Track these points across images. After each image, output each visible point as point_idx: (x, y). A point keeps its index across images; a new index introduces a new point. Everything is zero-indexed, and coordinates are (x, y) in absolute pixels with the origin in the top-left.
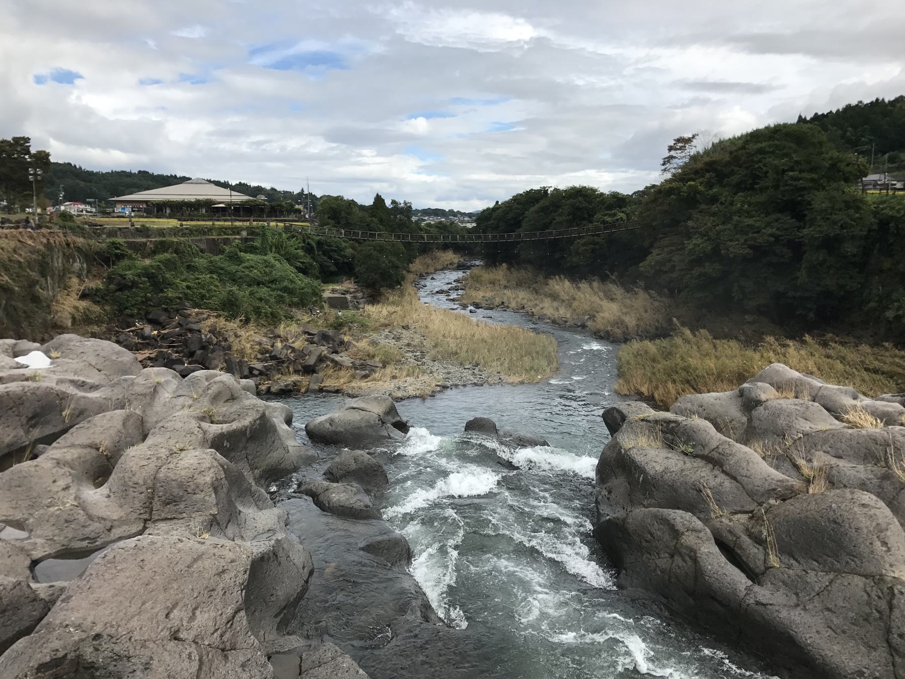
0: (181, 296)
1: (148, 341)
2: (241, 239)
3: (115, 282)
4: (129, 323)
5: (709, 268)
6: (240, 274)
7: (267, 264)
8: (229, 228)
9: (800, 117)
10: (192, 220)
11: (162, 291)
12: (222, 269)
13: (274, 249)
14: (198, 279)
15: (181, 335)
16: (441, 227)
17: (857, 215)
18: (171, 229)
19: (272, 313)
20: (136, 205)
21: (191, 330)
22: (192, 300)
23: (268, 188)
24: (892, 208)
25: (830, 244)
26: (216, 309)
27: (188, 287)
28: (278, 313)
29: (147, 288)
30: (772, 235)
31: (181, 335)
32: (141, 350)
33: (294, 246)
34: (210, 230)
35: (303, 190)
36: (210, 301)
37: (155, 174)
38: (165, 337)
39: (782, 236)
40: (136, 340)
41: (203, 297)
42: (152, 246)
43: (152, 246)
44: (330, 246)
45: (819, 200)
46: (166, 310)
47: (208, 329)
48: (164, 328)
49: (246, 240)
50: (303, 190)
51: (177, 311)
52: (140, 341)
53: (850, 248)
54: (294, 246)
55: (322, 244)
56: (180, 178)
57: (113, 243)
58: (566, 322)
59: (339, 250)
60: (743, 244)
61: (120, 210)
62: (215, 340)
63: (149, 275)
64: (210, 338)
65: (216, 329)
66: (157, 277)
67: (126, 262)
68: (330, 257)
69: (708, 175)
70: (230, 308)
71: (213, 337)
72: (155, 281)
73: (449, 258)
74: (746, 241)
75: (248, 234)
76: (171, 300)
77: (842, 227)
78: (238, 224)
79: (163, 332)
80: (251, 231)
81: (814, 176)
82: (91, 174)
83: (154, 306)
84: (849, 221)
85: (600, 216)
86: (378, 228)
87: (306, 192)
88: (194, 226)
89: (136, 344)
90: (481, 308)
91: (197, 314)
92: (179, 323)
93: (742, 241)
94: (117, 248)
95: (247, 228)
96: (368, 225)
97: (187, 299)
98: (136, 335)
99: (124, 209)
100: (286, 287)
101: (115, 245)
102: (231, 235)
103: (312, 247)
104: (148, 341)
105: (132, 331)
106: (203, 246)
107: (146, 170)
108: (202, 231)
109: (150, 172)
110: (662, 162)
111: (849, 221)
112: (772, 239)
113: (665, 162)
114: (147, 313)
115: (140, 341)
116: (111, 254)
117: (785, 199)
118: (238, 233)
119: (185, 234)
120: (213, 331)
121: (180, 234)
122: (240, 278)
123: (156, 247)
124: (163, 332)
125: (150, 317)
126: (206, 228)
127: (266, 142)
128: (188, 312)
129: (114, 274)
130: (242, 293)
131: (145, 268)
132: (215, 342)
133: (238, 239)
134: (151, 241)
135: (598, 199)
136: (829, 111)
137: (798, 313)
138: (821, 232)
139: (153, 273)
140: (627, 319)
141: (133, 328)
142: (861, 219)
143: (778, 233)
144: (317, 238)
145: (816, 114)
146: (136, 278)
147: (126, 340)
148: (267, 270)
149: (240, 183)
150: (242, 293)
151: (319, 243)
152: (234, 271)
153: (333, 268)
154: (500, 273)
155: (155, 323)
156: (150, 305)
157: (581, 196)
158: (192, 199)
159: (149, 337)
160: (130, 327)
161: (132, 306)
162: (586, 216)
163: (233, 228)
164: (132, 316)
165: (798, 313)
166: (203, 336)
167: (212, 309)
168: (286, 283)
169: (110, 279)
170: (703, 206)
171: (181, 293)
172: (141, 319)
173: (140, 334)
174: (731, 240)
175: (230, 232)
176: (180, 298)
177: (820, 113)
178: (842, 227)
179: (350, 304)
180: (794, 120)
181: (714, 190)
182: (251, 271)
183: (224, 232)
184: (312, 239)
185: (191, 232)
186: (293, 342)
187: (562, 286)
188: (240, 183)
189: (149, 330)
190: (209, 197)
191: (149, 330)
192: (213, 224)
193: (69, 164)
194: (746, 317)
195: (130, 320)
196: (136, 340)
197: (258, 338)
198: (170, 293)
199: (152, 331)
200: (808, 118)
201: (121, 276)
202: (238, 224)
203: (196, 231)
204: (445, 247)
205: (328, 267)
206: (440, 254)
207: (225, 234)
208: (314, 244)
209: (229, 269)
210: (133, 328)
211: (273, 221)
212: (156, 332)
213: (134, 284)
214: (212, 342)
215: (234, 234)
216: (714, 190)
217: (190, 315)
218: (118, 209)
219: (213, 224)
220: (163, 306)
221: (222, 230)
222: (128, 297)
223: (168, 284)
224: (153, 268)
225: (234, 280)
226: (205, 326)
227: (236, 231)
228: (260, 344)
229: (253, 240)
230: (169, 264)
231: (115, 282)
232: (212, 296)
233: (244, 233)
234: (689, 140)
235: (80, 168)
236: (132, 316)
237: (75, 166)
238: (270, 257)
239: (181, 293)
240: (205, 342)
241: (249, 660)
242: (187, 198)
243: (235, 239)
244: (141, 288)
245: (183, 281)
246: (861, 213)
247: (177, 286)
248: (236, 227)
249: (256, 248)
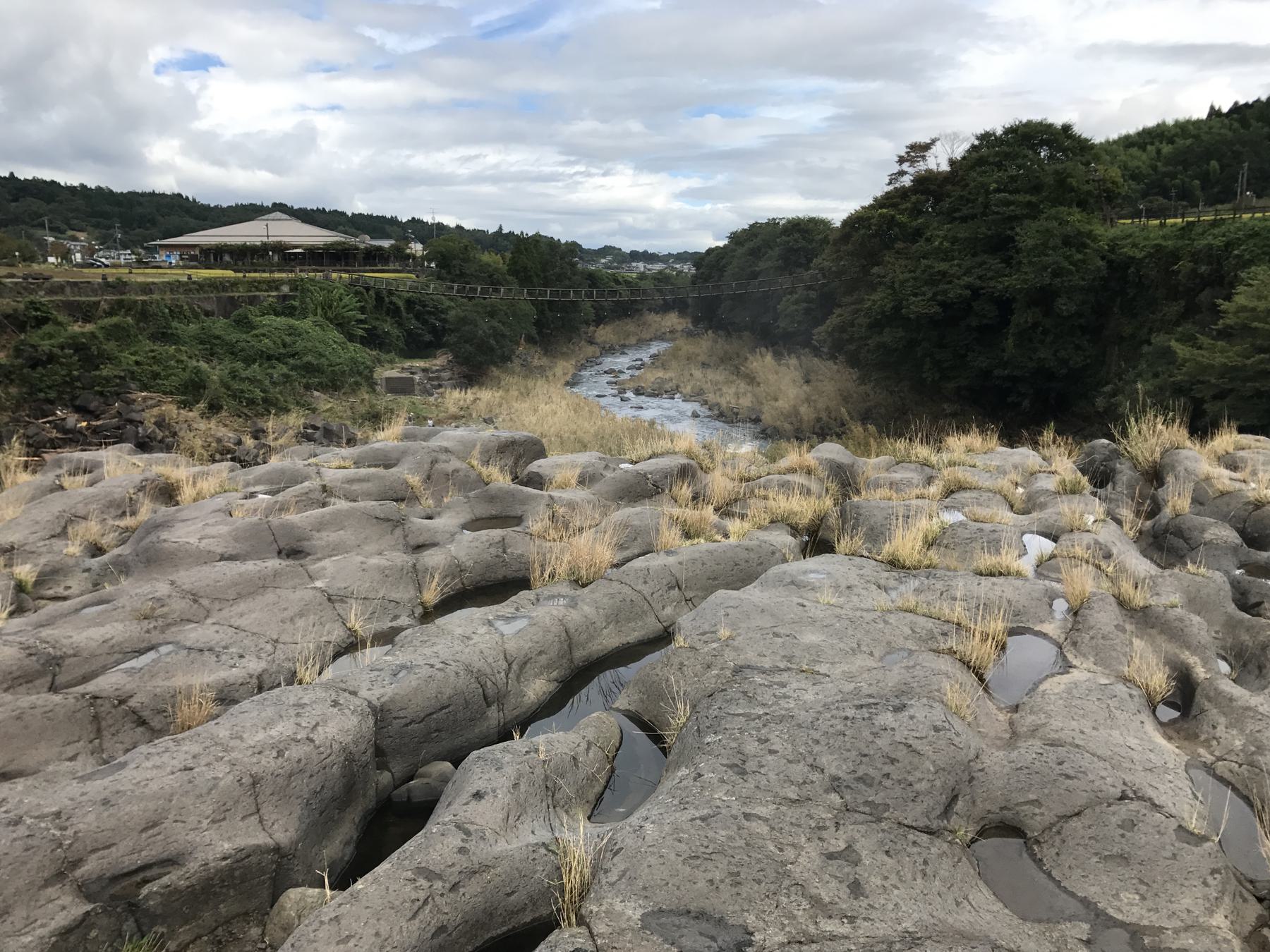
0: (122, 374)
1: (71, 436)
2: (278, 297)
3: (25, 354)
4: (43, 410)
5: (887, 337)
6: (244, 344)
7: (292, 331)
8: (264, 282)
9: (1212, 108)
10: (255, 271)
11: (97, 368)
12: (218, 337)
13: (319, 311)
14: (153, 351)
15: (119, 428)
16: (661, 278)
17: (1080, 256)
18: (168, 283)
19: (265, 400)
20: (185, 251)
21: (131, 421)
22: (140, 380)
23: (453, 225)
24: (1134, 245)
25: (1043, 298)
26: (172, 393)
27: (137, 363)
28: (277, 399)
29: (73, 364)
30: (968, 287)
31: (119, 428)
32: (60, 447)
33: (350, 306)
34: (234, 284)
35: (501, 228)
36: (165, 382)
37: (225, 205)
38: (98, 430)
39: (983, 288)
40: (54, 434)
41: (156, 376)
42: (106, 307)
43: (106, 307)
44: (424, 306)
45: (1027, 235)
46: (101, 394)
47: (153, 420)
48: (97, 418)
49: (285, 297)
50: (501, 228)
51: (118, 394)
52: (59, 435)
53: (1065, 306)
54: (350, 306)
55: (414, 303)
56: (330, 212)
57: (32, 303)
58: (737, 414)
59: (438, 311)
60: (929, 300)
61: (164, 258)
62: (160, 435)
63: (79, 347)
64: (153, 431)
65: (164, 420)
66: (90, 349)
67: (47, 328)
68: (425, 322)
69: (914, 198)
70: (192, 391)
71: (157, 431)
72: (84, 351)
73: (669, 324)
74: (935, 294)
75: (291, 290)
76: (107, 379)
77: (1055, 274)
78: (277, 275)
79: (94, 423)
80: (294, 284)
81: (1034, 199)
82: (207, 208)
83: (83, 388)
84: (1066, 264)
85: (820, 261)
86: (506, 280)
87: (505, 231)
88: (206, 279)
89: (51, 440)
90: (643, 394)
91: (145, 399)
92: (118, 412)
93: (930, 295)
94: (37, 309)
95: (290, 282)
96: (490, 276)
97: (133, 379)
98: (54, 428)
99: (169, 256)
100: (309, 363)
101: (33, 305)
102: (267, 291)
103: (398, 308)
104: (71, 436)
105: (49, 422)
106: (209, 307)
107: (283, 202)
108: (214, 285)
109: (289, 205)
110: (887, 181)
111: (1066, 264)
112: (968, 292)
113: (891, 180)
114: (74, 398)
115: (59, 435)
116: (29, 318)
117: (990, 233)
118: (277, 289)
119: (190, 290)
120: (160, 423)
121: (181, 290)
122: (242, 350)
123: (112, 308)
124: (94, 423)
125: (78, 403)
126: (228, 281)
127: (477, 157)
128: (133, 396)
129: (23, 345)
130: (215, 372)
131: (74, 337)
132: (159, 438)
133: (273, 296)
134: (106, 300)
135: (820, 237)
136: (1255, 99)
137: (1009, 400)
138: (1025, 281)
139: (83, 343)
140: (803, 409)
141: (50, 418)
142: (1084, 261)
143: (978, 282)
144: (406, 295)
145: (1236, 103)
146: (55, 350)
147: (37, 434)
148: (288, 339)
149: (413, 218)
150: (215, 372)
151: (409, 303)
152: (234, 340)
153: (428, 337)
154: (705, 344)
155: (83, 411)
156: (78, 387)
157: (799, 231)
158: (257, 241)
159: (73, 431)
160: (47, 416)
161: (50, 388)
162: (803, 261)
163: (269, 282)
164: (51, 402)
165: (1009, 400)
166: (140, 430)
167: (165, 393)
168: (309, 358)
169: (18, 352)
170: (899, 245)
171: (124, 370)
172: (65, 406)
173: (59, 426)
174: (916, 295)
175: (265, 287)
176: (121, 378)
177: (1242, 102)
178: (1055, 274)
179: (417, 388)
180: (1203, 114)
181: (919, 221)
182: (260, 341)
183: (256, 287)
184: (399, 297)
185: (201, 286)
186: (276, 439)
187: (763, 363)
188: (413, 218)
189: (72, 420)
190: (279, 239)
191: (73, 420)
192: (245, 276)
193: (180, 195)
194: (945, 406)
195: (46, 407)
196: (54, 434)
197: (222, 432)
198: (106, 371)
199: (78, 421)
200: (1225, 110)
201: (33, 346)
202: (277, 275)
203: (210, 286)
204: (665, 308)
205: (420, 335)
206: (652, 318)
207: (258, 289)
208: (401, 304)
209: (228, 338)
210: (50, 418)
211: (334, 271)
212: (84, 424)
213: (51, 358)
214: (155, 438)
215: (270, 289)
216: (919, 221)
217: (134, 401)
218: (161, 257)
219: (245, 276)
220: (96, 388)
221: (256, 285)
222: (43, 375)
223: (108, 359)
224: (85, 337)
225: (232, 353)
226: (149, 417)
227: (274, 285)
228: (219, 441)
229: (294, 298)
230: (117, 333)
231: (25, 354)
232: (170, 375)
233: (285, 289)
234: (926, 147)
235: (194, 200)
236: (51, 402)
237: (187, 198)
238: (306, 324)
239: (124, 370)
240: (143, 437)
241: (792, 823)
242: (250, 241)
243: (269, 296)
244: (62, 364)
245: (131, 354)
246: (1085, 254)
247: (120, 362)
248: (274, 281)
249: (294, 308)
